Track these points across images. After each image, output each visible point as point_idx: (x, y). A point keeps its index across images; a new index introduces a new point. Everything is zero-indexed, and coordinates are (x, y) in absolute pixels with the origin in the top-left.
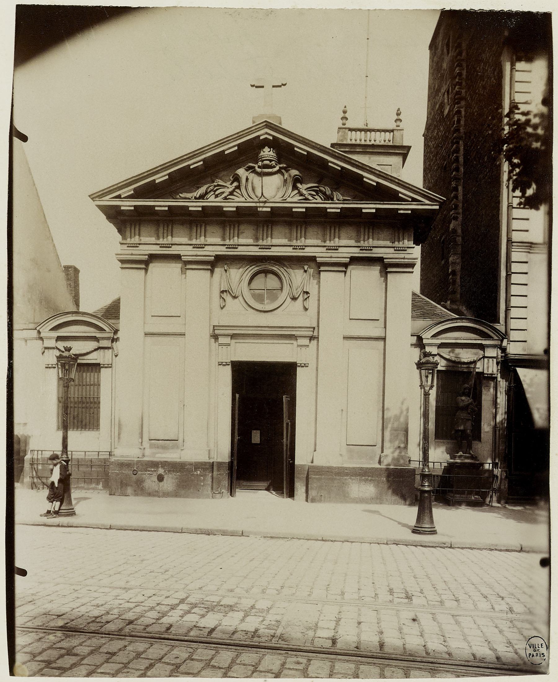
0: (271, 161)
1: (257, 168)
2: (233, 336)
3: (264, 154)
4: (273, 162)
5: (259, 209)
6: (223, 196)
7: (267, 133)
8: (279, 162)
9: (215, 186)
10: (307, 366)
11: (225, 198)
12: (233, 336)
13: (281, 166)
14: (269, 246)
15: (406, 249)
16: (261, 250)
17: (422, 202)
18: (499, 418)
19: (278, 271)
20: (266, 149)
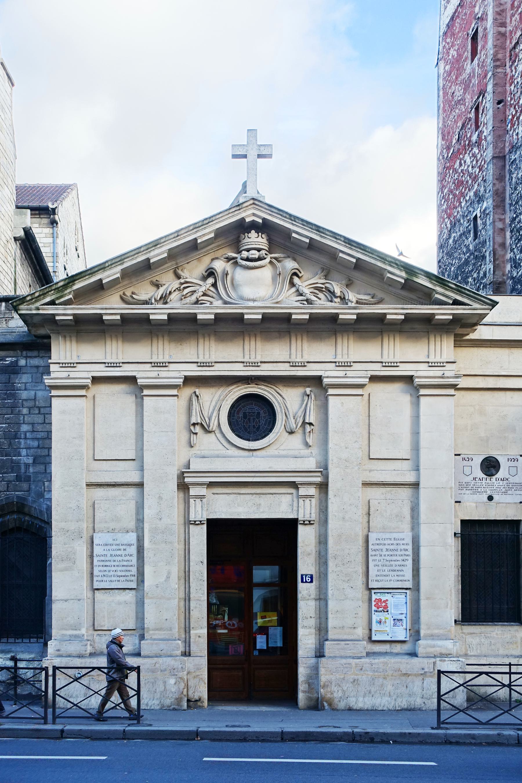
0: (259, 250)
1: (239, 261)
2: (211, 485)
3: (249, 240)
4: (263, 252)
5: (246, 317)
6: (193, 298)
7: (254, 215)
8: (270, 251)
9: (182, 284)
10: (313, 524)
11: (197, 302)
12: (211, 485)
13: (273, 255)
14: (203, 363)
15: (75, 365)
16: (200, 368)
17: (469, 305)
18: (414, 297)
19: (270, 396)
20: (253, 234)
